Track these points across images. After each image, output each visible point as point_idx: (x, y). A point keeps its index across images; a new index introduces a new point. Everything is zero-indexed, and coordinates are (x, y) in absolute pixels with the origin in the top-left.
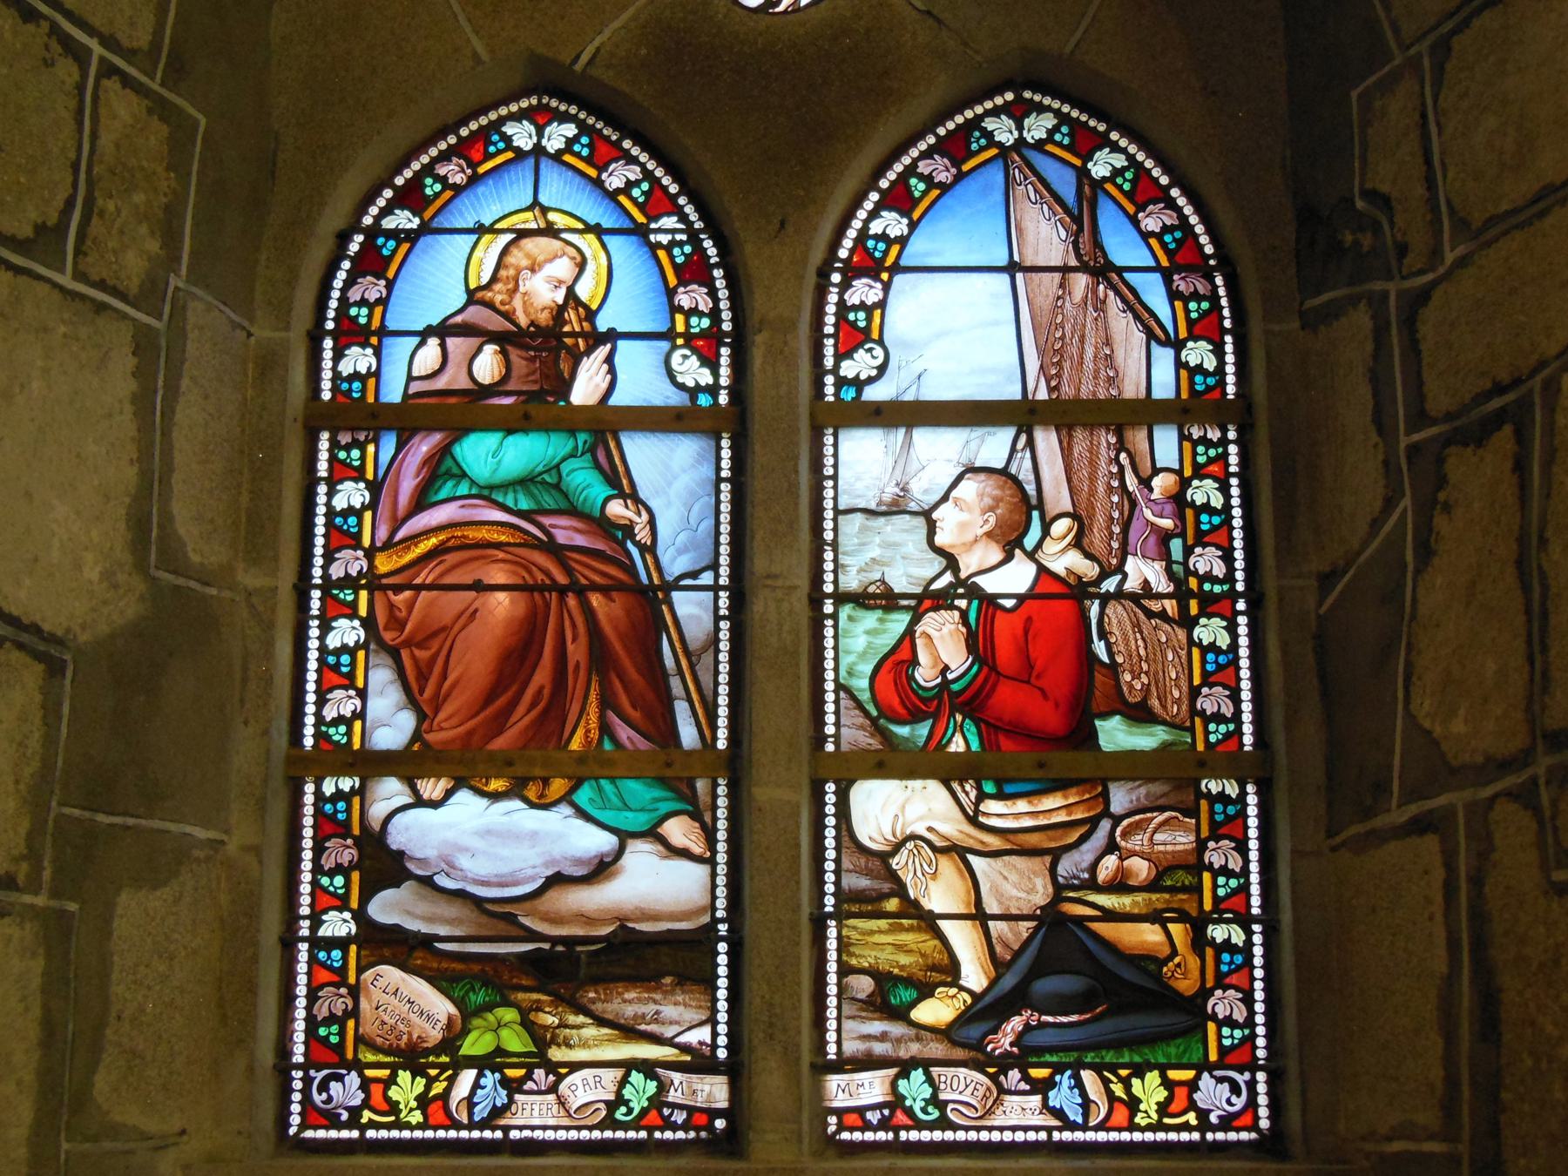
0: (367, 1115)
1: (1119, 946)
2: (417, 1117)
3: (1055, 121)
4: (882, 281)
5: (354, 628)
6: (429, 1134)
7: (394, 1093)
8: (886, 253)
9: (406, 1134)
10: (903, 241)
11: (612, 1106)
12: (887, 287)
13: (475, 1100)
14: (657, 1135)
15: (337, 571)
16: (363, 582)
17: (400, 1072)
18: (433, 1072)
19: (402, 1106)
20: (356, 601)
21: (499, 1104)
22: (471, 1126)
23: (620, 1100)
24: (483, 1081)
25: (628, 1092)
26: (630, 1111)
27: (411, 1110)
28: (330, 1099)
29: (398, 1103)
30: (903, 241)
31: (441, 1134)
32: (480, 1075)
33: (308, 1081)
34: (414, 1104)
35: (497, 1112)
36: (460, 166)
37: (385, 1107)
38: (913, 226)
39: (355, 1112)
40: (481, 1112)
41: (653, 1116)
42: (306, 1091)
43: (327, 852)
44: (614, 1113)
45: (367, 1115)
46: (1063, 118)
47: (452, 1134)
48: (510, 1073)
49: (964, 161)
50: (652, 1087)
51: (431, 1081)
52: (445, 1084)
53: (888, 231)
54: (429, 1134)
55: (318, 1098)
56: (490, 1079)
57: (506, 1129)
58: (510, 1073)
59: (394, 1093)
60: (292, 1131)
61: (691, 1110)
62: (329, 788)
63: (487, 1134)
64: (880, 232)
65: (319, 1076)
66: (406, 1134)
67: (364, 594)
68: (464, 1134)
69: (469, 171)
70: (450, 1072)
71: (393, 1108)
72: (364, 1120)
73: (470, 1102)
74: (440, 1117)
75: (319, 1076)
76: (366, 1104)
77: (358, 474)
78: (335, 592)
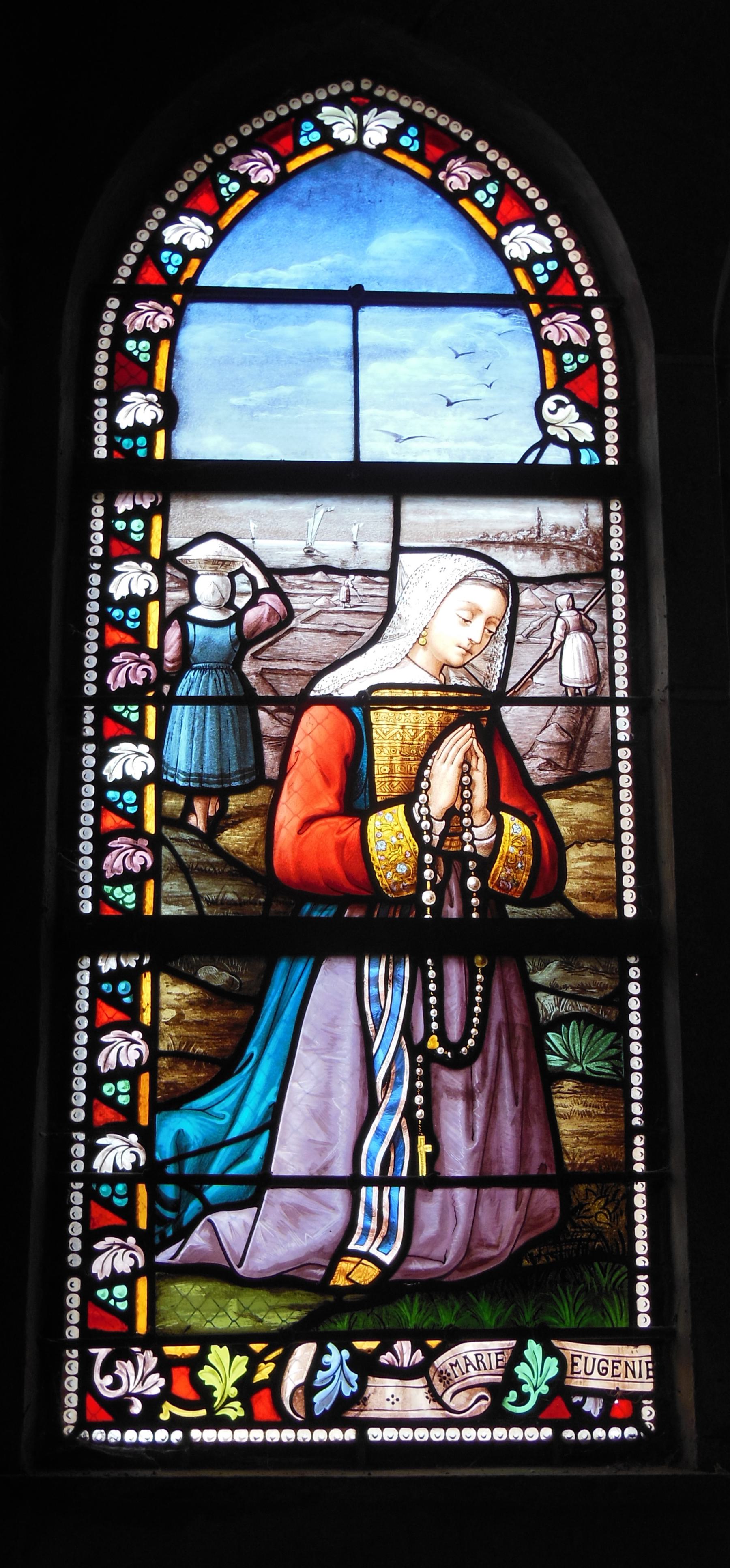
0: (167, 1410)
1: (232, 1200)
2: (234, 1411)
3: (401, 121)
4: (172, 304)
5: (140, 754)
6: (257, 1435)
7: (206, 1375)
8: (182, 268)
9: (225, 1436)
10: (204, 255)
11: (497, 1391)
12: (179, 314)
13: (317, 1384)
14: (568, 1434)
15: (116, 680)
16: (151, 694)
17: (214, 1348)
18: (257, 1347)
19: (216, 1394)
20: (143, 721)
21: (347, 1393)
22: (312, 1422)
23: (511, 1381)
24: (326, 1359)
25: (522, 1370)
26: (523, 1399)
27: (229, 1400)
28: (117, 1384)
29: (212, 1389)
30: (204, 255)
31: (273, 1435)
32: (322, 1351)
33: (87, 1362)
34: (233, 1392)
35: (342, 1403)
36: (265, 161)
37: (191, 1395)
38: (219, 237)
39: (152, 1404)
40: (322, 1401)
41: (558, 1409)
42: (85, 1376)
43: (105, 1051)
44: (501, 1400)
45: (167, 1410)
46: (410, 118)
47: (288, 1435)
48: (362, 1345)
49: (292, 157)
50: (552, 1367)
51: (255, 1361)
52: (271, 1367)
53: (185, 242)
54: (257, 1435)
55: (103, 1383)
56: (335, 1357)
57: (362, 1426)
58: (362, 1345)
59: (206, 1375)
60: (68, 1430)
61: (607, 1396)
62: (108, 964)
63: (336, 1434)
64: (175, 242)
65: (102, 1353)
66: (225, 1436)
67: (151, 712)
68: (304, 1435)
69: (277, 168)
70: (279, 1351)
71: (205, 1396)
72: (164, 1417)
73: (309, 1388)
74: (263, 1408)
75: (102, 1353)
76: (167, 1394)
77: (141, 552)
78: (117, 709)
